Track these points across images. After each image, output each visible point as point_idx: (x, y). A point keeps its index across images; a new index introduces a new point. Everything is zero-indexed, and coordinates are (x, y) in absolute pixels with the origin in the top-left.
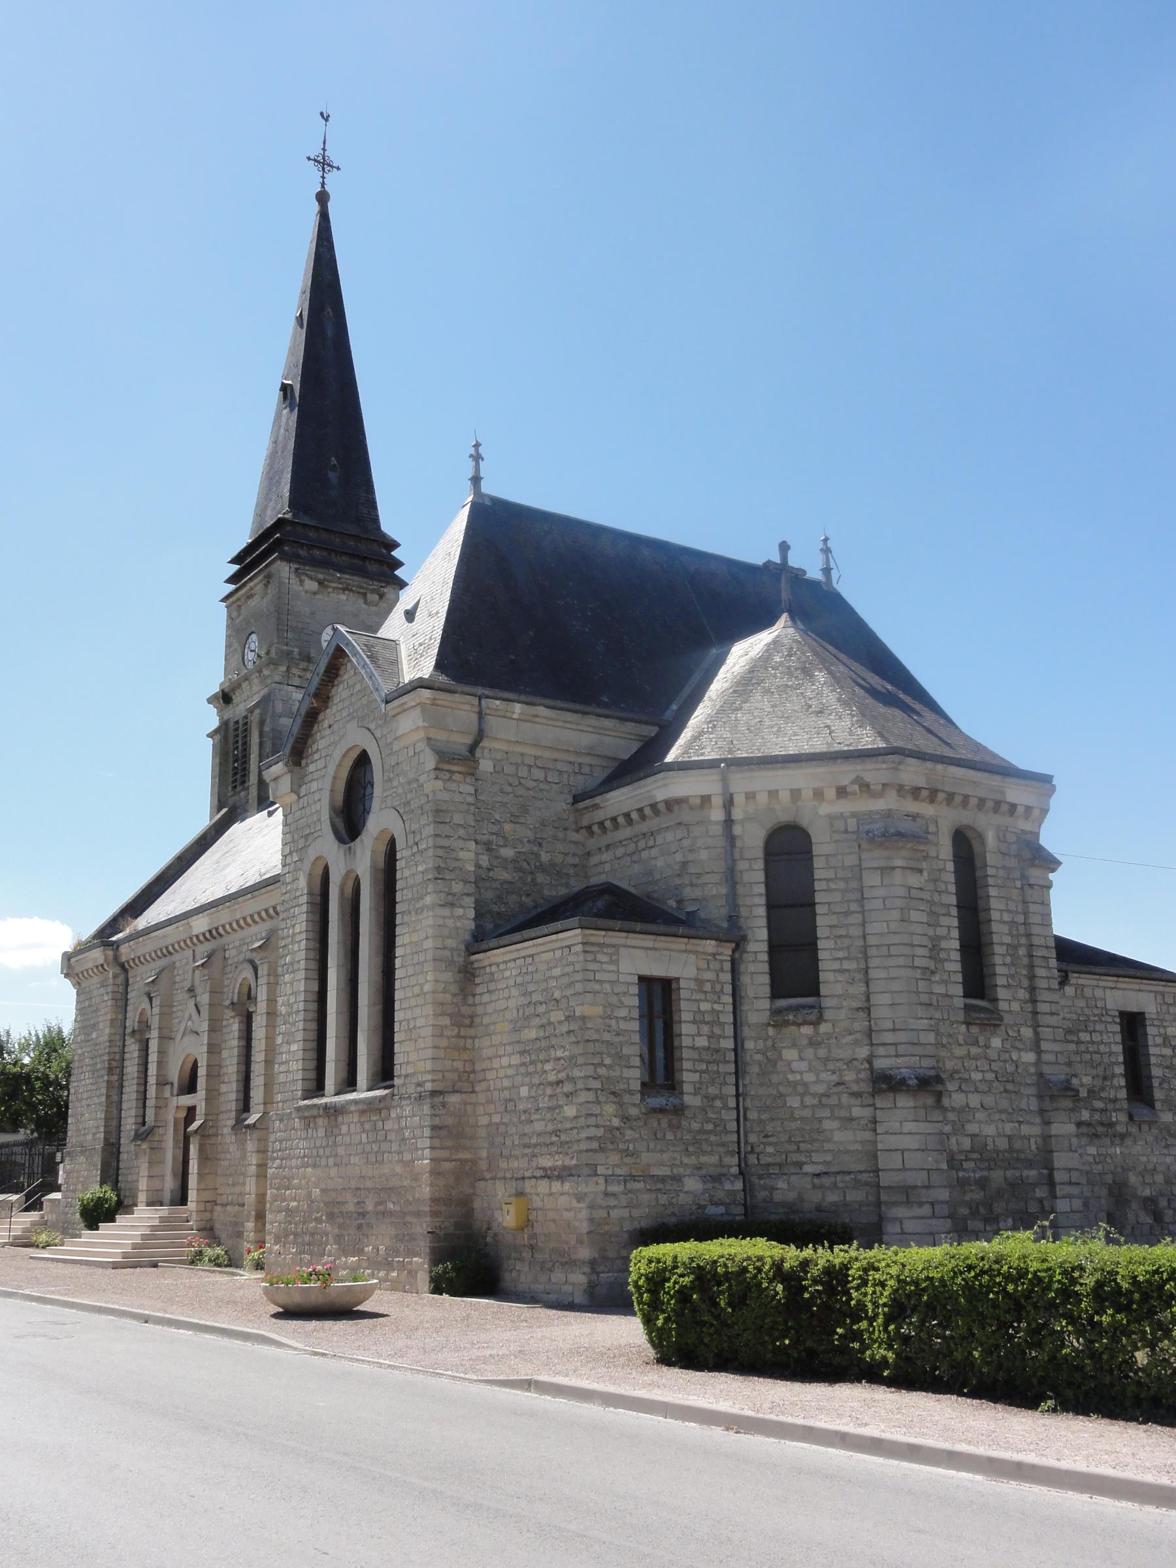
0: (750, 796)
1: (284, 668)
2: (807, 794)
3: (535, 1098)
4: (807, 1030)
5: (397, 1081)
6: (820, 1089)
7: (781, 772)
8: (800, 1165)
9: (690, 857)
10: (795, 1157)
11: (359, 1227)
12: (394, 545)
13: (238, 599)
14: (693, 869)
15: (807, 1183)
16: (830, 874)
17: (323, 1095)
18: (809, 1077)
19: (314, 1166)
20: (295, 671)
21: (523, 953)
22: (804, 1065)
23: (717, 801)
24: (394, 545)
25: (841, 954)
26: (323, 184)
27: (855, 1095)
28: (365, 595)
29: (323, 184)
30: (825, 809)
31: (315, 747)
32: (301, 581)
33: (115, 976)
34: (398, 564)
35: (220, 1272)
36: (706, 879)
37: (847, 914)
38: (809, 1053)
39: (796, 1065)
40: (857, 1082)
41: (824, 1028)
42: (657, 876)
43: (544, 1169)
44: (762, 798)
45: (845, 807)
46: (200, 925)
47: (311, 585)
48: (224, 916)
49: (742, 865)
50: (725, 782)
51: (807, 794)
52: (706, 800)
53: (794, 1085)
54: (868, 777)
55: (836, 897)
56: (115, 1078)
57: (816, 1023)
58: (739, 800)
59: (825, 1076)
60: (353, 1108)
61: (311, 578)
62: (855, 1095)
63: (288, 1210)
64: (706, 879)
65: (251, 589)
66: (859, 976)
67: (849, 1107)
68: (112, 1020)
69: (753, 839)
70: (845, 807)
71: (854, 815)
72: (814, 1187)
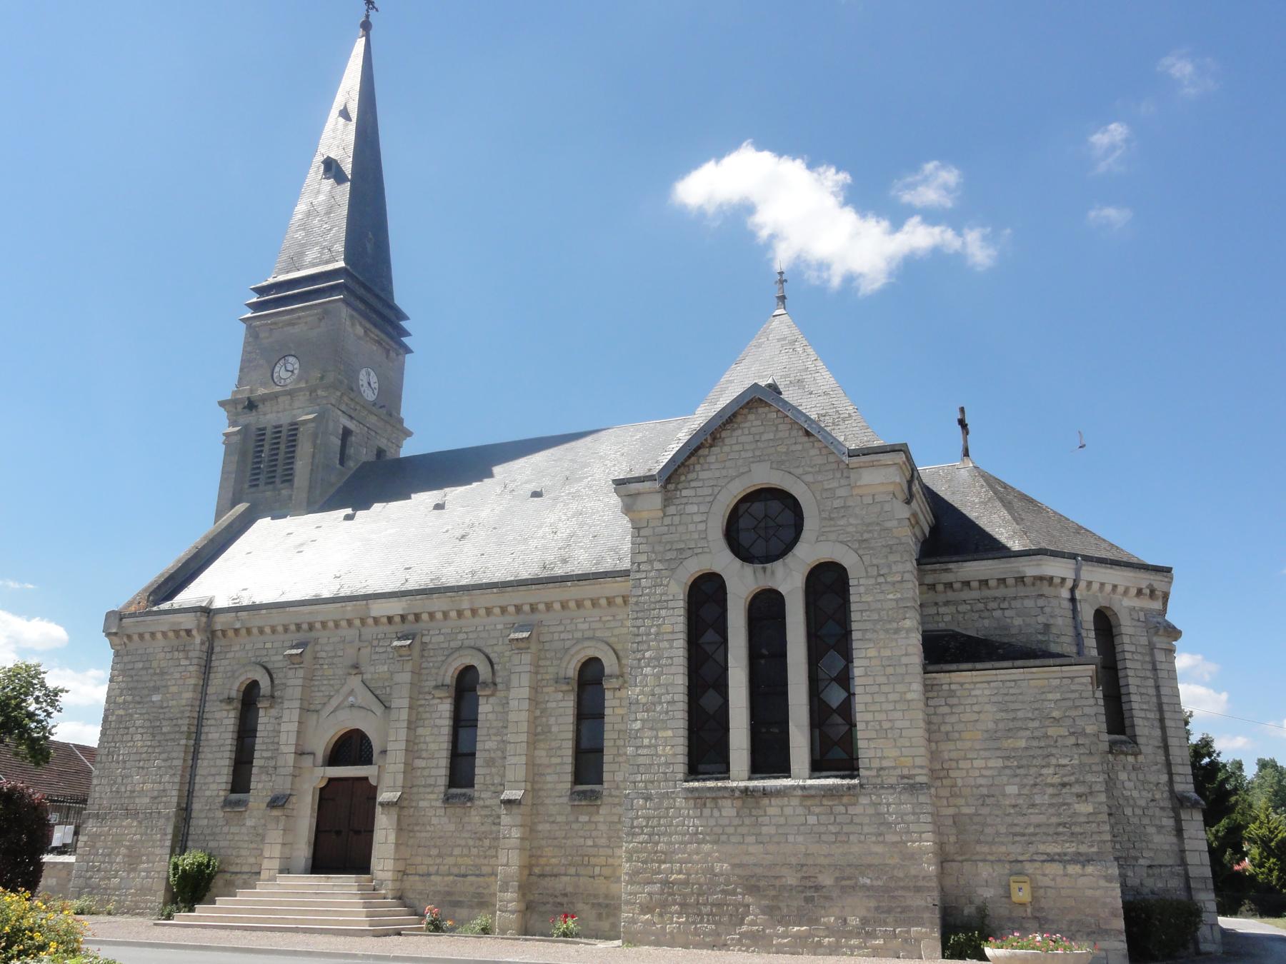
0: (1089, 584)
1: (339, 394)
2: (1121, 589)
3: (1029, 796)
4: (1131, 759)
5: (862, 772)
6: (1142, 803)
7: (1109, 571)
8: (1136, 859)
9: (1052, 621)
10: (1133, 853)
11: (808, 900)
12: (405, 318)
13: (275, 323)
14: (1054, 630)
15: (1144, 872)
16: (1133, 649)
17: (728, 778)
18: (1135, 794)
19: (715, 842)
20: (345, 398)
21: (1000, 678)
22: (1131, 785)
23: (1069, 584)
24: (405, 318)
25: (1145, 707)
26: (367, 16)
27: (1162, 809)
28: (388, 352)
29: (367, 16)
30: (1127, 602)
31: (692, 476)
32: (353, 325)
33: (202, 643)
34: (407, 334)
35: (567, 942)
36: (1063, 639)
37: (1146, 678)
38: (1133, 776)
39: (1127, 784)
40: (1163, 799)
41: (1141, 758)
42: (1014, 631)
43: (1048, 854)
44: (1095, 586)
45: (1137, 603)
46: (395, 608)
47: (360, 330)
48: (419, 605)
49: (1084, 633)
50: (1077, 571)
51: (1121, 589)
52: (1063, 580)
53: (1126, 798)
54: (1156, 585)
55: (1138, 665)
56: (192, 742)
57: (1135, 755)
58: (1082, 585)
59: (1144, 793)
60: (800, 792)
61: (361, 324)
62: (1162, 809)
63: (666, 883)
64: (1063, 639)
65: (299, 318)
66: (1157, 724)
67: (1160, 818)
68: (196, 685)
69: (1087, 615)
70: (1137, 603)
71: (1142, 609)
72: (1148, 875)
